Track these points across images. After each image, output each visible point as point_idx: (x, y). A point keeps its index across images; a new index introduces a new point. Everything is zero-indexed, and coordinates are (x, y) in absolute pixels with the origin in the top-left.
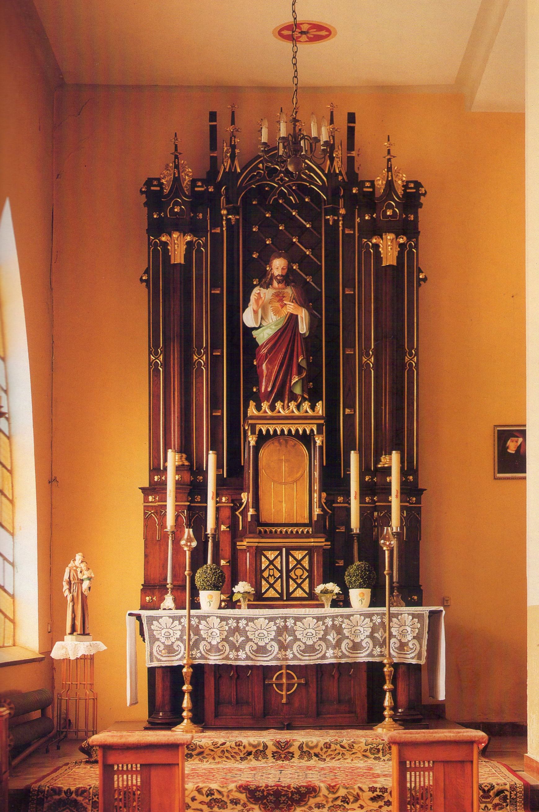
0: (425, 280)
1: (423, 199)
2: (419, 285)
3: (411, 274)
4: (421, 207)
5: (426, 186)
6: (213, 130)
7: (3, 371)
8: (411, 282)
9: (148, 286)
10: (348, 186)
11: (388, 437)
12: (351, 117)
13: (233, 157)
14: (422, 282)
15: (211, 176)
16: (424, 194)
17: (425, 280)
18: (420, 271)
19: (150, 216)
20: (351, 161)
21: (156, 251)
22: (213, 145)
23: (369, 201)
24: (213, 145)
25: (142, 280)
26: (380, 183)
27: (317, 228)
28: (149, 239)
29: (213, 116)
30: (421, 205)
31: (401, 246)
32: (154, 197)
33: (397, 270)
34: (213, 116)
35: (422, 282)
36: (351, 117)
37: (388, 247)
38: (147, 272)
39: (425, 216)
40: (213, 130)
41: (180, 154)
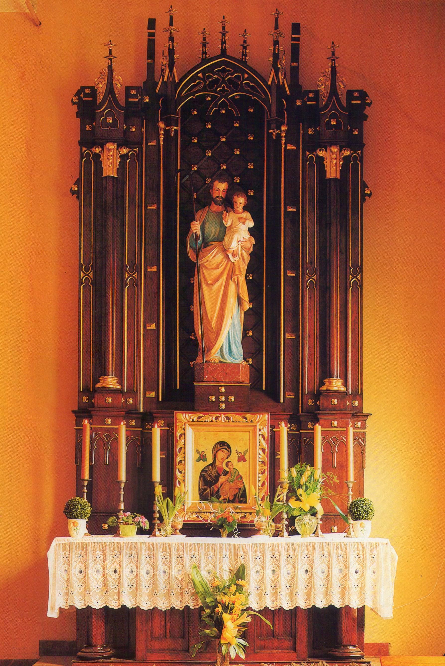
0: (370, 195)
1: (368, 111)
2: (363, 200)
3: (355, 191)
4: (366, 120)
5: (372, 96)
6: (151, 43)
7: (251, 665)
8: (355, 200)
9: (78, 198)
10: (291, 100)
11: (277, 622)
12: (296, 28)
13: (171, 65)
14: (367, 198)
15: (149, 86)
16: (369, 105)
17: (370, 195)
18: (364, 186)
19: (82, 128)
20: (295, 71)
21: (88, 162)
22: (151, 55)
23: (312, 115)
24: (151, 55)
25: (73, 193)
26: (324, 89)
27: (259, 140)
28: (81, 149)
29: (152, 23)
30: (366, 117)
31: (346, 159)
32: (86, 105)
33: (341, 183)
34: (152, 23)
35: (367, 198)
36: (296, 28)
37: (333, 161)
38: (78, 182)
39: (371, 130)
40: (151, 43)
41: (114, 57)
